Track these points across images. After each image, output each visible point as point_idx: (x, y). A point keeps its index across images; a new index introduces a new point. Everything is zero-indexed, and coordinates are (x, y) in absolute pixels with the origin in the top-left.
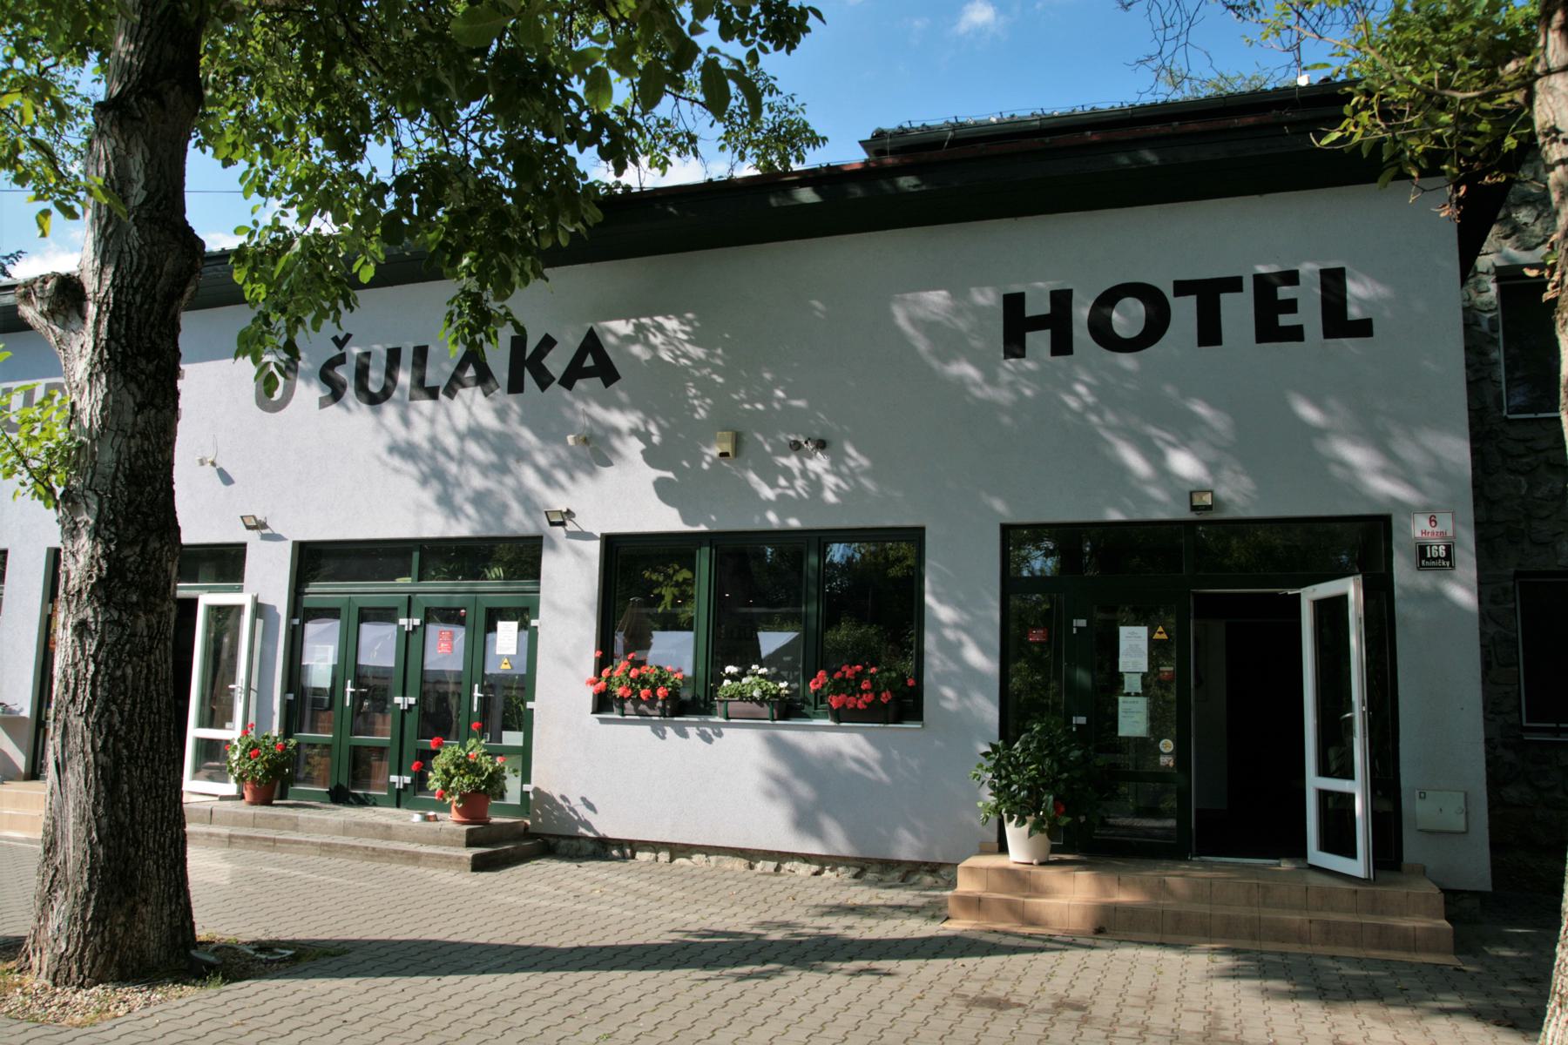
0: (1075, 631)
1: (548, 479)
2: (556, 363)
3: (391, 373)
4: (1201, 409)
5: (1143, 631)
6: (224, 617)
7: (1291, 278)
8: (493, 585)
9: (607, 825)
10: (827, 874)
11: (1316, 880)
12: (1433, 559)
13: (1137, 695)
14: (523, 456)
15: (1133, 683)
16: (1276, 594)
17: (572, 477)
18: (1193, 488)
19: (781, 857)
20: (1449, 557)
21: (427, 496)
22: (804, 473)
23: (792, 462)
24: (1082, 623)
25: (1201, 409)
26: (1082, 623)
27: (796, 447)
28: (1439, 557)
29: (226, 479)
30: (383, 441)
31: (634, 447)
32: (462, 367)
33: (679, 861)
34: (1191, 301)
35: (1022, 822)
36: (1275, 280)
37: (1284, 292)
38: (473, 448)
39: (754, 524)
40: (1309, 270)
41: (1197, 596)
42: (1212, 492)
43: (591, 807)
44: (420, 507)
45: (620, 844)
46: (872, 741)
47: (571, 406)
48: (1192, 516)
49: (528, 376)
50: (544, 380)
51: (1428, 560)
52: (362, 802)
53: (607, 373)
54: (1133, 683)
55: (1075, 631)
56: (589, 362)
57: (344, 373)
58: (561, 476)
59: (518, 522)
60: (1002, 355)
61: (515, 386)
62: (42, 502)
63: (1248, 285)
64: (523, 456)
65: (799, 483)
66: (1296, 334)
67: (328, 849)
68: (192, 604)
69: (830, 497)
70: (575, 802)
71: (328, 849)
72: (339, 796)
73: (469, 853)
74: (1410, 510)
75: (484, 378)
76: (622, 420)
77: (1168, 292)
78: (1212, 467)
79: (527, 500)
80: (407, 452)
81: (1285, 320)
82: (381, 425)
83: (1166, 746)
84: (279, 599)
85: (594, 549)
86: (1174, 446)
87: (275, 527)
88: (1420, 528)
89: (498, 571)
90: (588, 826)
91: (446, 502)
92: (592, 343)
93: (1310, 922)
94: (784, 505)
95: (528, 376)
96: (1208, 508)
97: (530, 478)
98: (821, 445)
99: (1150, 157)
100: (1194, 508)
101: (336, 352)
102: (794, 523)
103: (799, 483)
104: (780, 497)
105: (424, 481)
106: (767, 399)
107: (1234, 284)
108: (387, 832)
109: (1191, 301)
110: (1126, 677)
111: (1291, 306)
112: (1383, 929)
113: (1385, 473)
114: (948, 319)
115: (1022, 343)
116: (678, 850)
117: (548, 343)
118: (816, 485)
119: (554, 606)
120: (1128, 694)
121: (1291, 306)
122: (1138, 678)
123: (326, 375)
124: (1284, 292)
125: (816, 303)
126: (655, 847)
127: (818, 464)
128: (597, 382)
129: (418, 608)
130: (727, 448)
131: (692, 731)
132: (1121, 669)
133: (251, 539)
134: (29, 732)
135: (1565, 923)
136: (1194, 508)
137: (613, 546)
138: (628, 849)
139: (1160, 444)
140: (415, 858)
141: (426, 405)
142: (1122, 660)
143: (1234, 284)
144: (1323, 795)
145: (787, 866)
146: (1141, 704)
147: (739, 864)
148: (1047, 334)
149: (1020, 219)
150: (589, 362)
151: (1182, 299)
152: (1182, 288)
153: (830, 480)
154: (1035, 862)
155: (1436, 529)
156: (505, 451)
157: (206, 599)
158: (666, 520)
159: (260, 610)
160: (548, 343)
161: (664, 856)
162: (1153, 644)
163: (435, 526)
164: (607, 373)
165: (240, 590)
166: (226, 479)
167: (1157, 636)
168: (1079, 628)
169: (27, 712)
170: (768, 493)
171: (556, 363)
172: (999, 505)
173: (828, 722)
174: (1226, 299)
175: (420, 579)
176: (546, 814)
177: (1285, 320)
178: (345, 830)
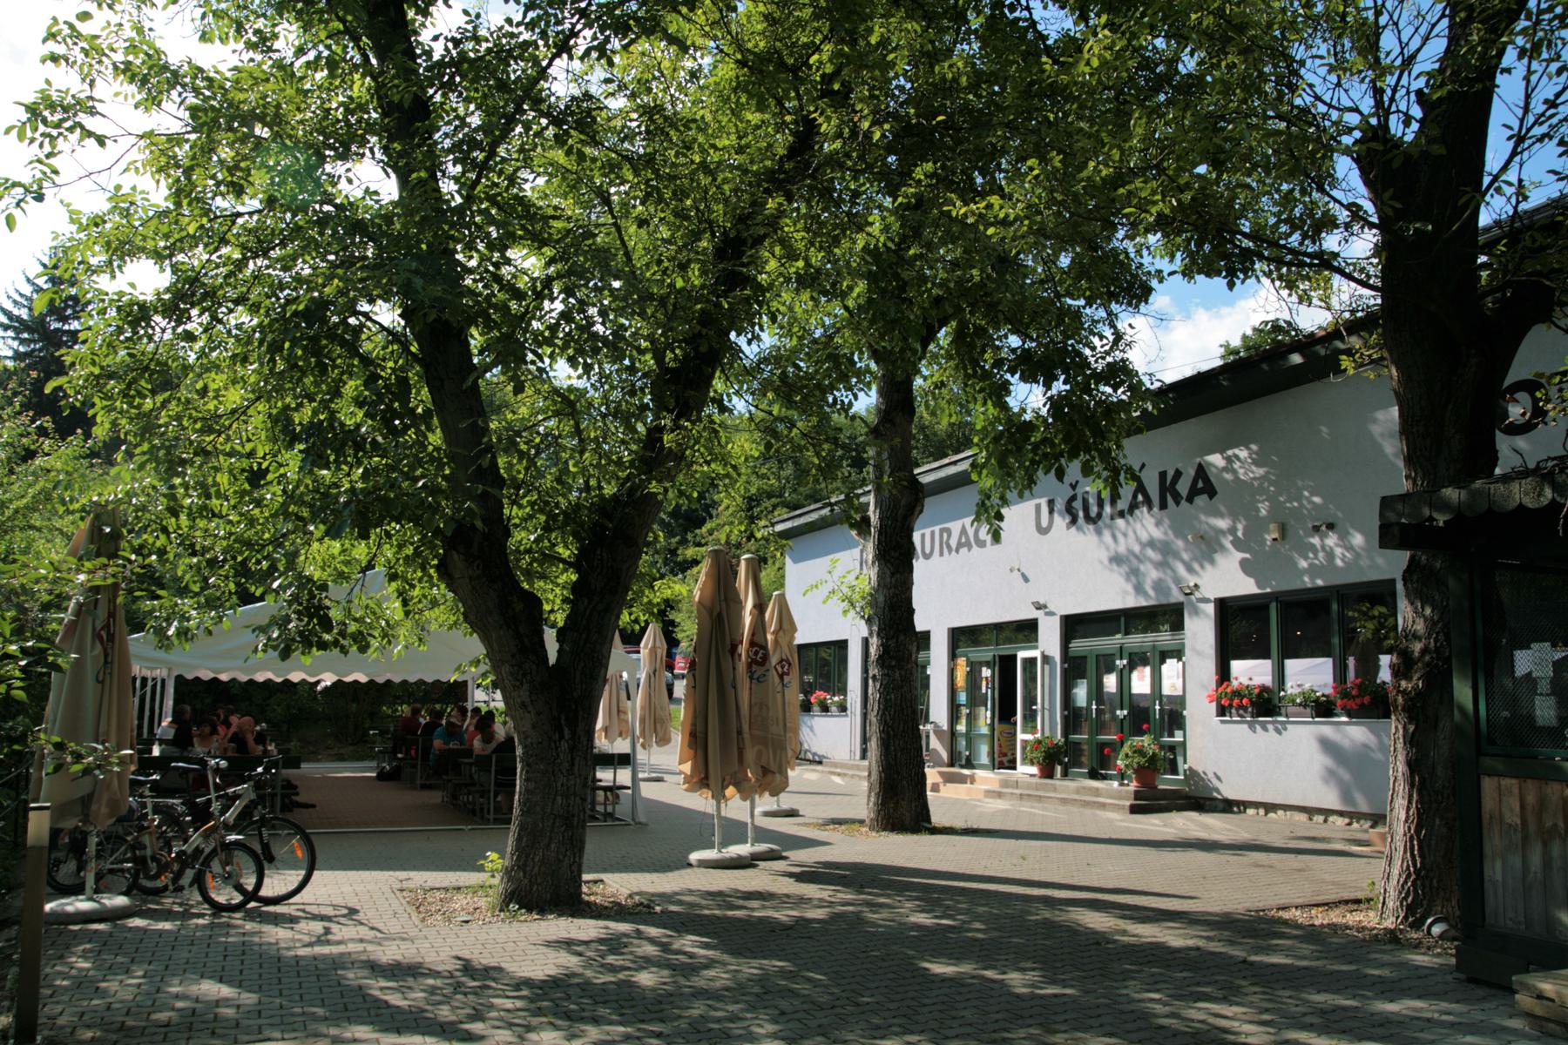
1: (1190, 569)
2: (1183, 487)
3: (1101, 504)
6: (1031, 663)
8: (1164, 638)
9: (1229, 791)
10: (1355, 825)
14: (1177, 556)
17: (1202, 567)
19: (1327, 813)
21: (1129, 588)
22: (1323, 547)
23: (1316, 541)
27: (1316, 529)
29: (1026, 579)
30: (1104, 556)
31: (1227, 542)
32: (1135, 497)
33: (1272, 815)
38: (1150, 552)
39: (1296, 585)
43: (1219, 778)
44: (1125, 592)
45: (1238, 803)
46: (1372, 731)
47: (1197, 518)
49: (1169, 498)
50: (1177, 498)
52: (1104, 778)
53: (1211, 491)
56: (1200, 484)
57: (1078, 504)
58: (1196, 566)
59: (1176, 596)
61: (1163, 506)
64: (1177, 556)
65: (1321, 555)
67: (1064, 801)
68: (1014, 657)
69: (1339, 563)
70: (1211, 775)
71: (1064, 801)
72: (1094, 775)
73: (1128, 803)
75: (1148, 502)
76: (1223, 524)
79: (1177, 580)
80: (1116, 559)
82: (1101, 541)
84: (1055, 652)
85: (1210, 609)
87: (1051, 608)
89: (1167, 627)
90: (1218, 791)
91: (1139, 589)
92: (1201, 471)
94: (1313, 570)
95: (1169, 498)
97: (1181, 570)
98: (1331, 527)
101: (1071, 493)
102: (1320, 582)
103: (1321, 555)
104: (1311, 565)
105: (1128, 579)
106: (1299, 498)
108: (1097, 792)
116: (1270, 807)
117: (1178, 474)
118: (1330, 555)
119: (1193, 649)
123: (1069, 509)
125: (1324, 429)
126: (1256, 805)
127: (1331, 540)
128: (1205, 497)
129: (1125, 654)
130: (1275, 535)
131: (1270, 727)
133: (1038, 614)
134: (947, 737)
135: (403, 1040)
137: (1223, 605)
138: (1242, 806)
140: (1103, 806)
141: (1120, 522)
145: (1331, 819)
147: (1303, 817)
150: (1200, 484)
153: (1338, 551)
156: (1165, 549)
157: (1022, 655)
158: (1246, 586)
159: (1046, 659)
160: (1178, 474)
161: (1262, 812)
163: (1131, 601)
164: (1211, 491)
165: (1036, 648)
166: (1026, 579)
169: (945, 728)
170: (1303, 564)
171: (1183, 487)
173: (1344, 719)
175: (1127, 633)
176: (1196, 784)
178: (1078, 791)
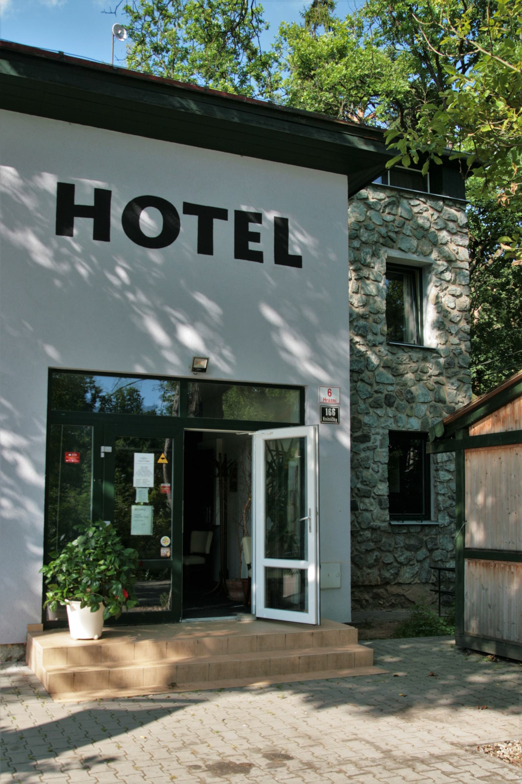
0: (103, 455)
4: (202, 299)
5: (151, 457)
7: (258, 218)
11: (262, 630)
12: (330, 417)
13: (145, 504)
15: (142, 496)
16: (234, 434)
18: (195, 355)
20: (337, 416)
24: (109, 449)
25: (202, 299)
26: (109, 449)
28: (332, 416)
34: (194, 219)
35: (433, 618)
36: (252, 217)
37: (253, 227)
40: (270, 216)
41: (187, 432)
42: (208, 359)
48: (190, 375)
51: (326, 417)
54: (142, 496)
55: (103, 455)
60: (259, 225)
62: (252, 40)
63: (231, 216)
66: (258, 257)
74: (320, 384)
77: (180, 210)
78: (208, 342)
81: (252, 246)
83: (165, 541)
86: (183, 323)
88: (323, 395)
93: (299, 658)
96: (203, 370)
99: (193, 106)
100: (194, 370)
107: (222, 214)
109: (194, 219)
110: (138, 490)
111: (256, 237)
112: (338, 656)
113: (312, 360)
114: (15, 194)
115: (71, 225)
120: (138, 504)
121: (256, 237)
122: (146, 492)
124: (253, 227)
132: (135, 485)
136: (194, 370)
139: (173, 320)
142: (136, 478)
143: (222, 214)
144: (268, 570)
146: (148, 511)
148: (90, 221)
149: (72, 124)
151: (188, 216)
152: (189, 209)
154: (96, 637)
155: (331, 398)
162: (158, 467)
167: (160, 461)
168: (106, 453)
172: (51, 351)
174: (217, 222)
177: (252, 246)
